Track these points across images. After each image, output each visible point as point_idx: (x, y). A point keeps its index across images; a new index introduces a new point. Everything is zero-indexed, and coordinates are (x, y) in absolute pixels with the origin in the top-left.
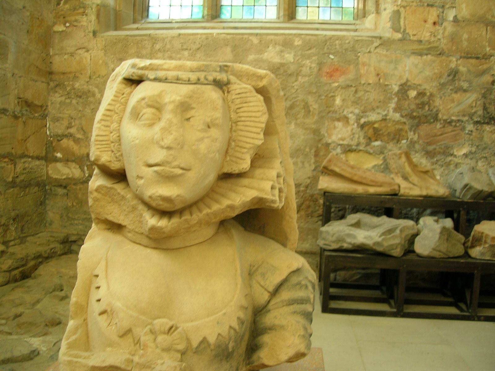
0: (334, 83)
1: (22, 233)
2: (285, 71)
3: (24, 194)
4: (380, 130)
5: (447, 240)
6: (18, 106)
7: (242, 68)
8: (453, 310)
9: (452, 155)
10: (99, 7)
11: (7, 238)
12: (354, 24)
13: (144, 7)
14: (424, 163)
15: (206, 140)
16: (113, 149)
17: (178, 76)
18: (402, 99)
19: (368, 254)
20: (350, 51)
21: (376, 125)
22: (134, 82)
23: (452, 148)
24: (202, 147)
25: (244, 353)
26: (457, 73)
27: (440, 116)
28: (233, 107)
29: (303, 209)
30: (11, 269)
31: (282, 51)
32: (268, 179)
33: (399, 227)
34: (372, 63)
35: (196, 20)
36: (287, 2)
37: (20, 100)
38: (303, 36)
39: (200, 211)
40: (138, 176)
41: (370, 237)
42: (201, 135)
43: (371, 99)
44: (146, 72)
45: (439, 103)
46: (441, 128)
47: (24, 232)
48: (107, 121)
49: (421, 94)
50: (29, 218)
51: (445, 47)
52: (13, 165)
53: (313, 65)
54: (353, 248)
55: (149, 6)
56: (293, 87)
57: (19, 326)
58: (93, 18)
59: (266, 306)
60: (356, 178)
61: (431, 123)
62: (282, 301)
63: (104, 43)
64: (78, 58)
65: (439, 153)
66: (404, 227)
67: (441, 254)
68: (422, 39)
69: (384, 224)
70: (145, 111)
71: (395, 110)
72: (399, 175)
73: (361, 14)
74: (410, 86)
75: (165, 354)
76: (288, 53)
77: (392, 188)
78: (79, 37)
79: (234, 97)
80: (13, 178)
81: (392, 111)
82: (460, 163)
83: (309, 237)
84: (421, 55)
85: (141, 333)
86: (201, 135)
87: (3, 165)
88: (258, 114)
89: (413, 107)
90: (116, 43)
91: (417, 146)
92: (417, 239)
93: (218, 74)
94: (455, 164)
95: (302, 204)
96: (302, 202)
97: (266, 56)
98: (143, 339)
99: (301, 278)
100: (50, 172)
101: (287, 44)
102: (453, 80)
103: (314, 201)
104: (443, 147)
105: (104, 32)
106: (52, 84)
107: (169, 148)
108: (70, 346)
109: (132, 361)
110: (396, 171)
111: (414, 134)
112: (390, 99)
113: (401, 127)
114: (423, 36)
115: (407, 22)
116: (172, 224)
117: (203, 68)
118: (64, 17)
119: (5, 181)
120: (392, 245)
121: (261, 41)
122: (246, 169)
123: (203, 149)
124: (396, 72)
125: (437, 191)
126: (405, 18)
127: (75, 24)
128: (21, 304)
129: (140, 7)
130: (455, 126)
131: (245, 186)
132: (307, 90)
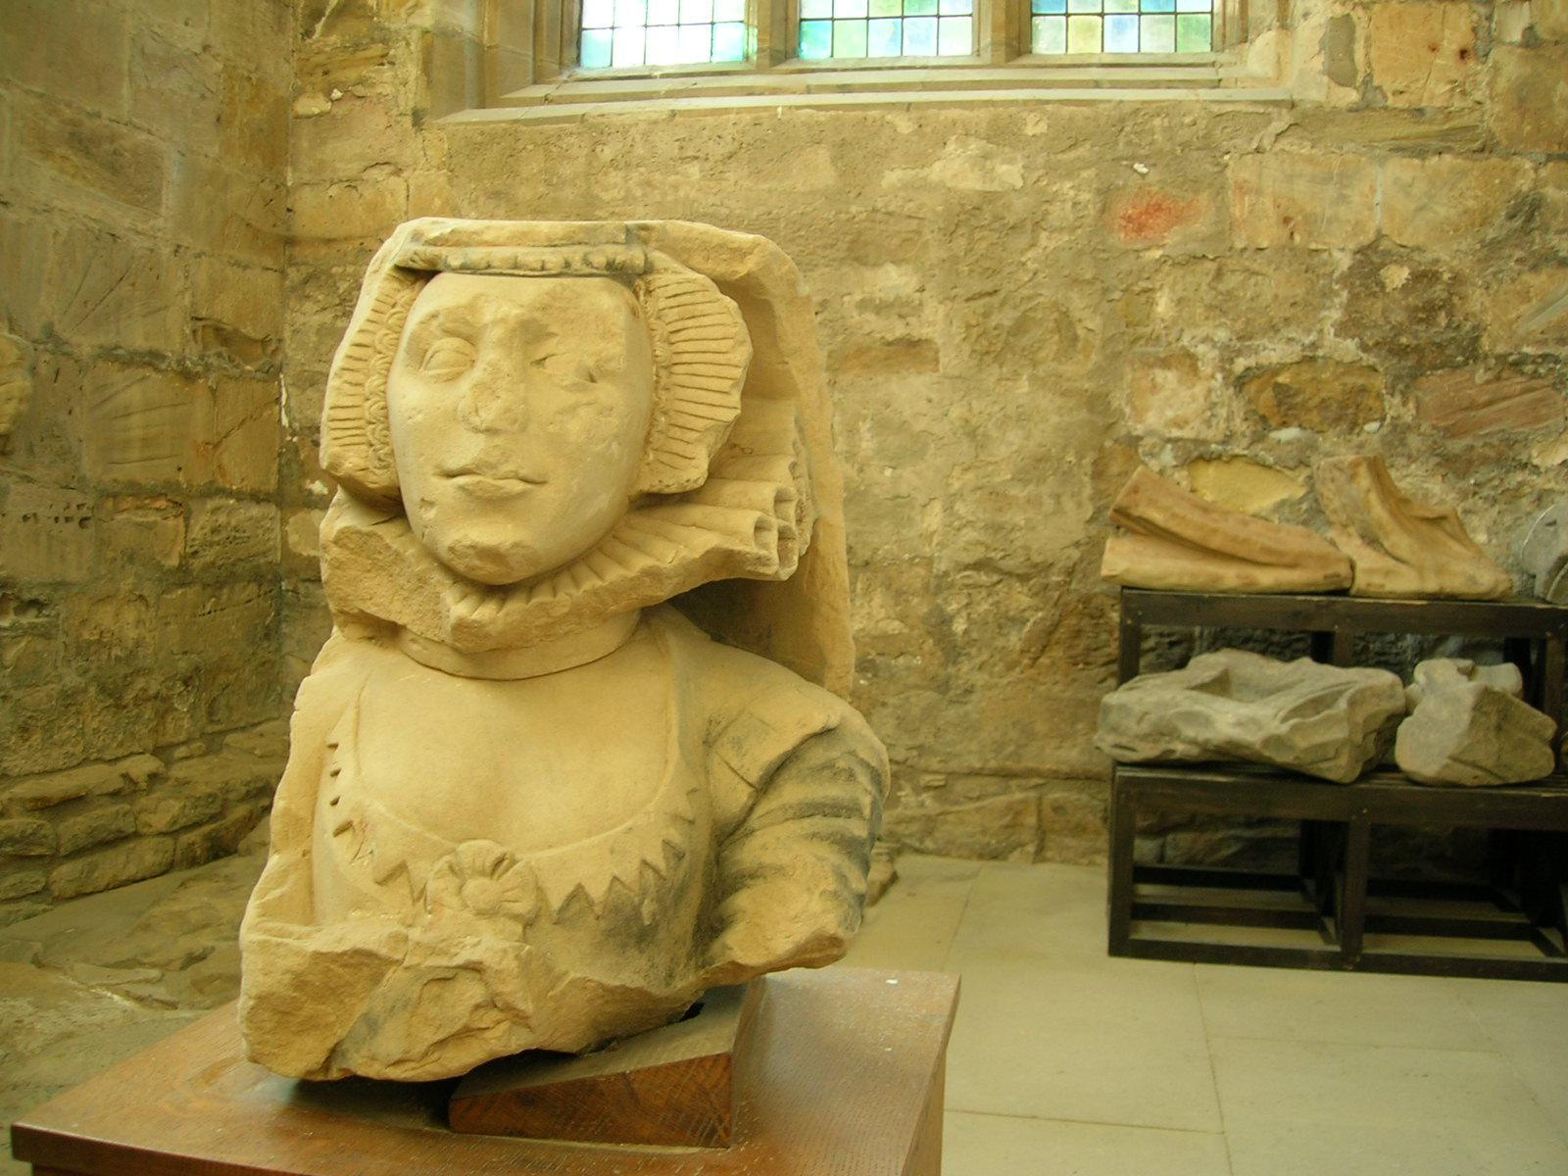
0: (1148, 249)
1: (212, 721)
2: (998, 218)
3: (216, 604)
4: (1296, 394)
5: (1499, 728)
6: (193, 343)
7: (690, 231)
8: (1525, 951)
9: (1524, 466)
10: (428, 36)
11: (167, 737)
12: (1213, 64)
13: (566, 32)
14: (1438, 492)
15: (582, 412)
16: (371, 438)
17: (516, 257)
18: (1363, 295)
19: (1249, 775)
20: (1198, 149)
21: (1281, 379)
22: (417, 274)
23: (1526, 443)
24: (574, 427)
25: (689, 936)
26: (1539, 207)
27: (1485, 344)
28: (661, 330)
29: (1057, 643)
30: (177, 827)
31: (986, 157)
32: (752, 507)
33: (1346, 690)
34: (1267, 184)
35: (725, 69)
36: (1003, 4)
37: (200, 324)
38: (1049, 107)
39: (577, 584)
40: (423, 500)
41: (1254, 722)
42: (571, 398)
43: (1267, 298)
44: (443, 251)
45: (1482, 304)
46: (1488, 382)
47: (216, 718)
48: (357, 371)
49: (1424, 277)
50: (232, 677)
51: (1496, 128)
52: (181, 520)
53: (1085, 196)
54: (1203, 758)
55: (580, 29)
56: (1024, 264)
57: (198, 986)
58: (412, 70)
59: (744, 820)
60: (1215, 543)
61: (1456, 367)
62: (784, 808)
63: (446, 146)
64: (368, 193)
65: (1485, 460)
66: (1362, 691)
67: (1478, 773)
68: (1423, 105)
69: (1302, 681)
70: (437, 344)
71: (1342, 329)
72: (1352, 530)
73: (1234, 31)
74: (1387, 253)
75: (483, 924)
76: (1004, 162)
77: (1330, 571)
78: (371, 131)
79: (662, 304)
80: (183, 557)
81: (1332, 331)
82: (1552, 491)
83: (1080, 726)
84: (1421, 153)
85: (428, 872)
86: (571, 398)
87: (152, 518)
88: (724, 345)
89: (1398, 317)
90: (481, 144)
91: (1414, 441)
92: (1402, 729)
93: (620, 248)
94: (1535, 496)
95: (1056, 626)
96: (1056, 618)
97: (936, 172)
98: (431, 887)
99: (834, 754)
100: (293, 538)
101: (1002, 132)
102: (1525, 231)
103: (1092, 617)
104: (1495, 441)
105: (448, 112)
106: (294, 275)
107: (491, 431)
108: (266, 912)
109: (406, 939)
110: (1344, 517)
111: (1404, 404)
112: (1327, 294)
113: (1361, 381)
114: (1426, 95)
115: (1374, 53)
116: (507, 615)
117: (581, 236)
118: (326, 73)
119: (159, 566)
120: (1323, 746)
121: (920, 126)
122: (695, 481)
123: (578, 431)
124: (1342, 210)
125: (1472, 579)
126: (1368, 39)
127: (360, 90)
128: (205, 926)
129: (558, 36)
130: (1535, 375)
131: (694, 525)
132: (1066, 272)
